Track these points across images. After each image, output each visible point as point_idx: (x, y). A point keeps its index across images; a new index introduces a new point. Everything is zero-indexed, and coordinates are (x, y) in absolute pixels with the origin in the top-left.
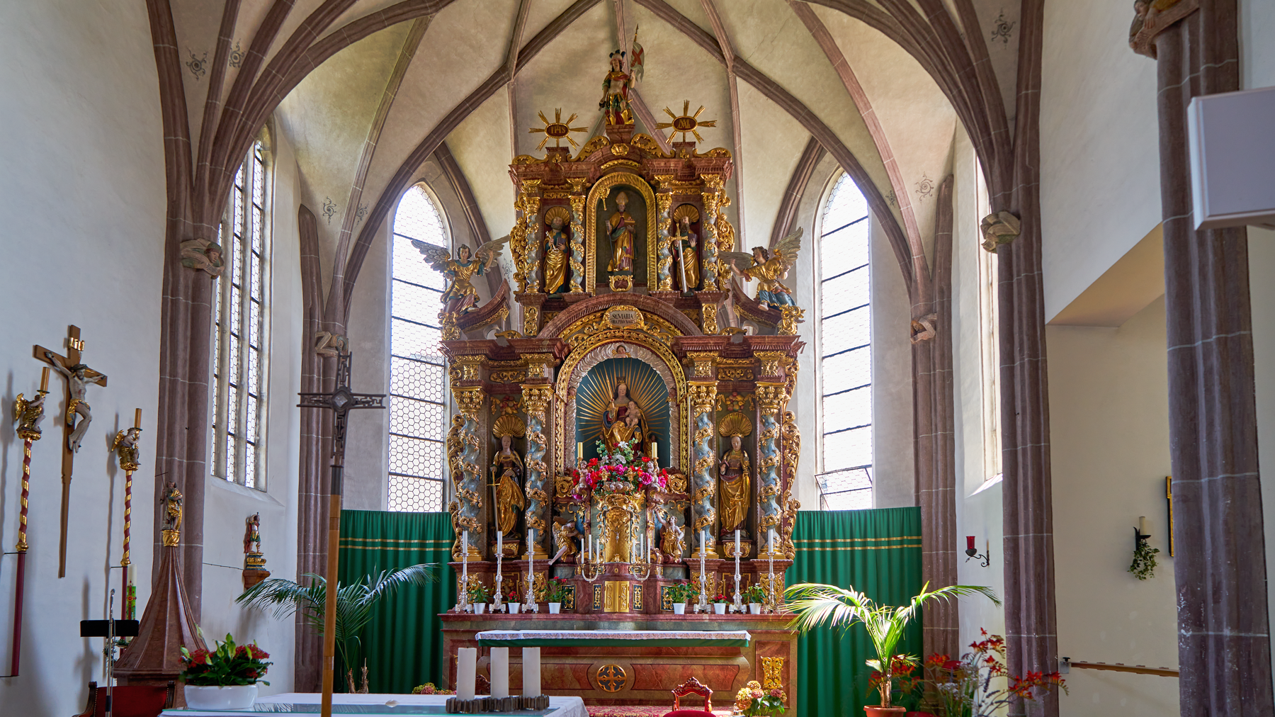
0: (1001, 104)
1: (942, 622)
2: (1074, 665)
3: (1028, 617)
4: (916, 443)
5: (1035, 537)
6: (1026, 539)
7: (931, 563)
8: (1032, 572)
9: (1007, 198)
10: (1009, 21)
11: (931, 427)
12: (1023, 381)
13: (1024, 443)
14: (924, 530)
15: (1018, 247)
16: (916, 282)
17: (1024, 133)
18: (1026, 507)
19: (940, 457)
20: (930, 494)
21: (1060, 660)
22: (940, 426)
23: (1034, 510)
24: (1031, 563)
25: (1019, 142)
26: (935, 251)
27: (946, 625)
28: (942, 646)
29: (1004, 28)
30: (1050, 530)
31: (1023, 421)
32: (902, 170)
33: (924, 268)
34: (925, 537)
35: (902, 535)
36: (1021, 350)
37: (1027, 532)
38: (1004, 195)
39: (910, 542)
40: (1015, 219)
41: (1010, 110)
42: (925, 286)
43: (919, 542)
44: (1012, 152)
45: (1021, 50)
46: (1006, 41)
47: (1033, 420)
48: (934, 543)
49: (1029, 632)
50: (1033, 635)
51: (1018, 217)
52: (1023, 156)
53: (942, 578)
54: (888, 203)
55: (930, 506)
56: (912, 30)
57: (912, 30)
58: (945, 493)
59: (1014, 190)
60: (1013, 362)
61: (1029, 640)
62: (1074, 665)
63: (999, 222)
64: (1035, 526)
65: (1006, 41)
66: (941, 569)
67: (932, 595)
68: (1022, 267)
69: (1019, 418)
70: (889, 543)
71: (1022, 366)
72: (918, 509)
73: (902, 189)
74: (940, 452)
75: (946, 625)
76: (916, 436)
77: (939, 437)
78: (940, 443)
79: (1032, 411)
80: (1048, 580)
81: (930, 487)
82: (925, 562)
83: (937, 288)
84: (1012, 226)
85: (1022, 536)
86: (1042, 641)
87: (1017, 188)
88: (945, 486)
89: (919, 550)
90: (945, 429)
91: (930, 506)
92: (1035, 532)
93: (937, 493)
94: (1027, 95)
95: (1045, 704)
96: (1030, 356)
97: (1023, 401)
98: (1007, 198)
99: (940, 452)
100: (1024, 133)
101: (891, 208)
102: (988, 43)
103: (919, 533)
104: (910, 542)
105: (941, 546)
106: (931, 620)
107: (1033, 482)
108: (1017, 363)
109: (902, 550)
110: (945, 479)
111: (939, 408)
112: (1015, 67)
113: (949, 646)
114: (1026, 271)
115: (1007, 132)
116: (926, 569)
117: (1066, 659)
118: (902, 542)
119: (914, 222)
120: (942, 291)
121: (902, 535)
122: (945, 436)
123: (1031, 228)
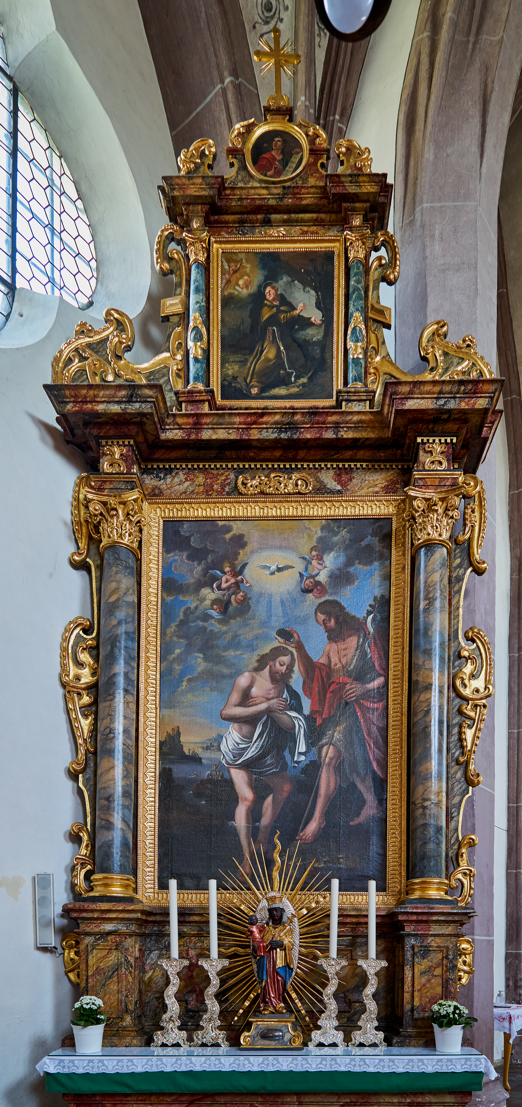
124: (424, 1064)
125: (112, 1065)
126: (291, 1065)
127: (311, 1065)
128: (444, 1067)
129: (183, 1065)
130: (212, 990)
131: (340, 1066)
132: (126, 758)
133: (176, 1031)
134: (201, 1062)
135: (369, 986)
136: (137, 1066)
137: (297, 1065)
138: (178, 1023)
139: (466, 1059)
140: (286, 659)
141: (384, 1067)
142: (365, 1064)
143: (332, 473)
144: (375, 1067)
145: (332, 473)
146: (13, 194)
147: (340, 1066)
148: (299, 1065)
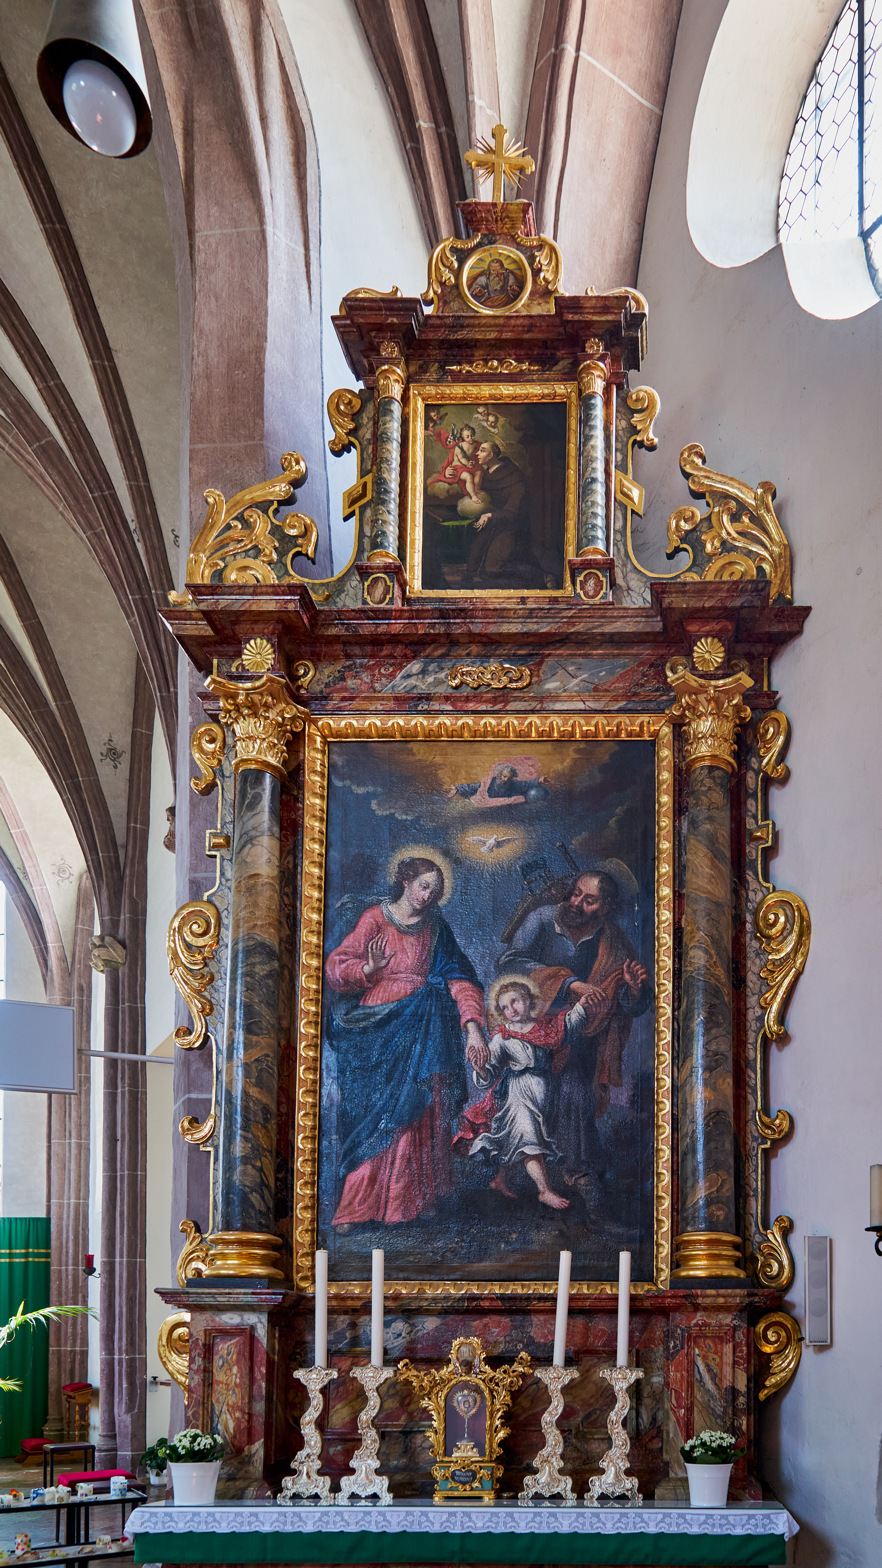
0: (111, 828)
1: (69, 1342)
2: (162, 1384)
3: (120, 1339)
4: (49, 1148)
5: (128, 1262)
6: (121, 1263)
7: (60, 1279)
8: (124, 1296)
9: (115, 924)
10: (119, 749)
11: (65, 1133)
12: (123, 1108)
13: (122, 1170)
14: (54, 1243)
15: (124, 975)
16: (51, 971)
17: (132, 865)
18: (122, 1233)
19: (73, 1167)
20: (61, 1206)
21: (149, 1379)
22: (74, 1133)
23: (129, 1236)
24: (124, 1287)
25: (128, 872)
26: (75, 944)
27: (74, 1345)
28: (68, 1367)
29: (113, 754)
30: (144, 1255)
31: (122, 1147)
32: (36, 846)
33: (63, 959)
34: (54, 1251)
35: (27, 1248)
36: (123, 1078)
37: (121, 1256)
38: (111, 920)
39: (38, 1255)
40: (120, 946)
41: (120, 838)
42: (63, 978)
43: (48, 1255)
44: (122, 879)
45: (131, 781)
46: (116, 767)
47: (130, 1148)
48: (64, 1258)
49: (120, 1354)
50: (124, 1356)
51: (124, 947)
52: (131, 887)
53: (70, 1295)
54: (21, 876)
55: (60, 1218)
56: (17, 712)
57: (17, 712)
58: (77, 1206)
59: (122, 917)
60: (116, 1089)
61: (120, 1361)
62: (162, 1384)
63: (105, 946)
64: (128, 1252)
65: (116, 767)
66: (70, 1285)
67: (30, 1316)
68: (126, 997)
69: (119, 1143)
70: (10, 1256)
71: (123, 1093)
72: (48, 1220)
73: (35, 866)
74: (73, 1162)
75: (74, 1345)
76: (49, 1141)
77: (73, 1145)
78: (74, 1151)
79: (130, 1139)
80: (140, 1303)
81: (61, 1197)
82: (53, 1277)
83: (75, 984)
84: (118, 954)
85: (117, 1260)
86: (131, 1362)
87: (125, 917)
88: (78, 1198)
89: (47, 1265)
90: (79, 1136)
91: (60, 1218)
92: (128, 1257)
93: (69, 1204)
94: (135, 828)
95: (132, 1421)
96: (130, 1086)
97: (123, 1128)
98: (115, 924)
99: (73, 1162)
100: (132, 865)
101: (24, 882)
102: (96, 762)
103: (48, 1246)
104: (38, 1255)
105: (70, 1261)
106: (58, 1340)
107: (129, 1208)
108: (119, 1090)
109: (26, 1264)
110: (79, 1190)
111: (74, 1113)
112: (126, 796)
113: (77, 1366)
114: (129, 1001)
115: (117, 858)
116: (54, 1286)
117: (155, 1378)
118: (26, 1255)
119: (50, 906)
120: (81, 989)
121: (27, 1248)
122: (79, 1146)
123: (137, 960)
124: (599, 1521)
125: (231, 1519)
126: (619, 1525)
127: (604, 1524)
128: (160, 1525)
129: (674, 1525)
130: (311, 1415)
131: (691, 1526)
132: (230, 1004)
133: (314, 1476)
134: (566, 1520)
135: (311, 1409)
136: (433, 1524)
137: (584, 1524)
138: (318, 1464)
139: (364, 1512)
140: (429, 877)
141: (670, 1525)
142: (686, 1521)
143: (212, 278)
144: (700, 1525)
145: (212, 278)
146: (861, 141)
147: (691, 1526)
148: (588, 1524)
